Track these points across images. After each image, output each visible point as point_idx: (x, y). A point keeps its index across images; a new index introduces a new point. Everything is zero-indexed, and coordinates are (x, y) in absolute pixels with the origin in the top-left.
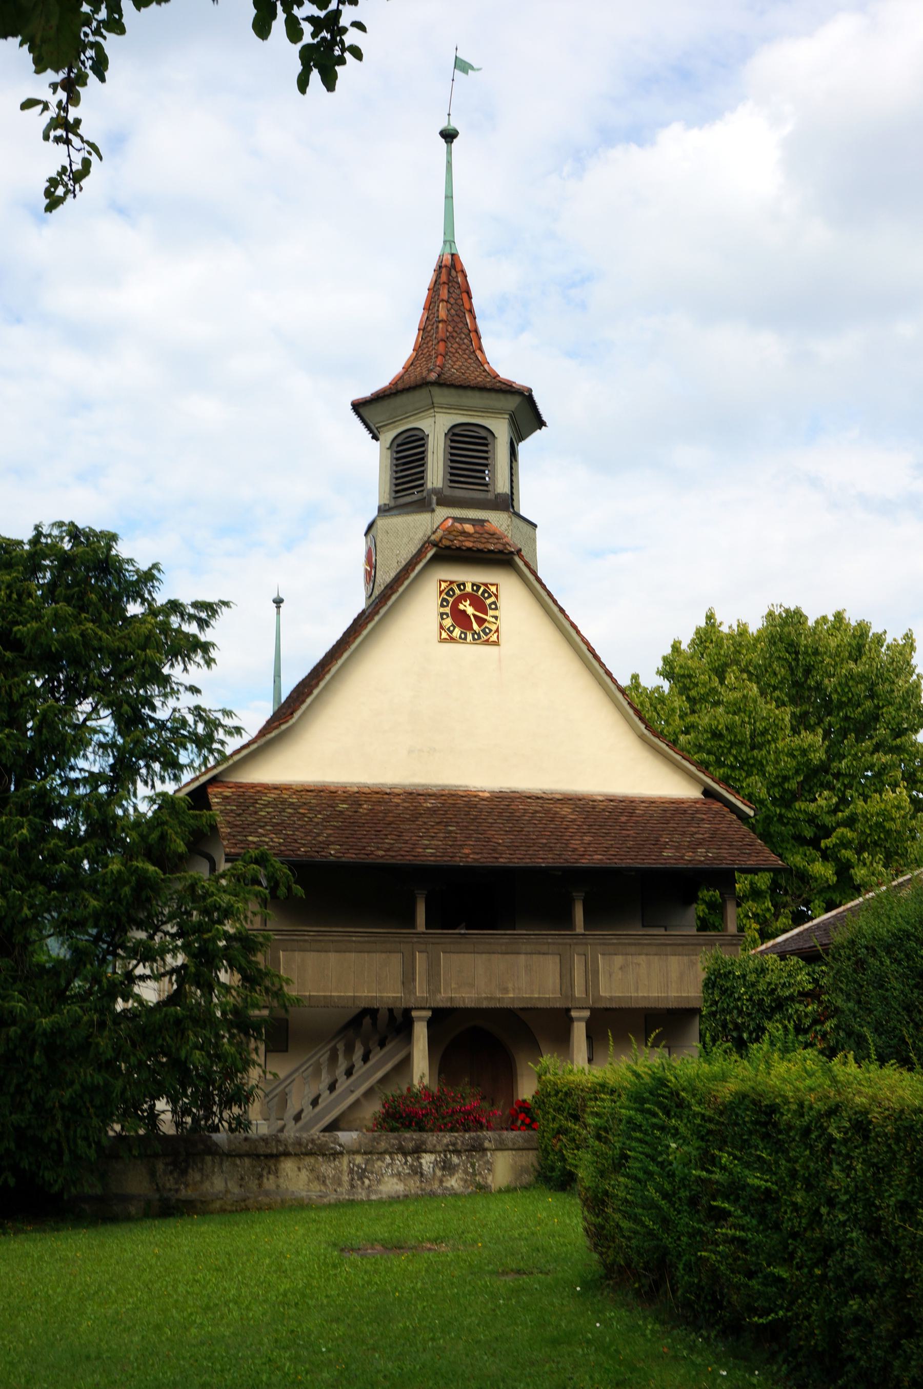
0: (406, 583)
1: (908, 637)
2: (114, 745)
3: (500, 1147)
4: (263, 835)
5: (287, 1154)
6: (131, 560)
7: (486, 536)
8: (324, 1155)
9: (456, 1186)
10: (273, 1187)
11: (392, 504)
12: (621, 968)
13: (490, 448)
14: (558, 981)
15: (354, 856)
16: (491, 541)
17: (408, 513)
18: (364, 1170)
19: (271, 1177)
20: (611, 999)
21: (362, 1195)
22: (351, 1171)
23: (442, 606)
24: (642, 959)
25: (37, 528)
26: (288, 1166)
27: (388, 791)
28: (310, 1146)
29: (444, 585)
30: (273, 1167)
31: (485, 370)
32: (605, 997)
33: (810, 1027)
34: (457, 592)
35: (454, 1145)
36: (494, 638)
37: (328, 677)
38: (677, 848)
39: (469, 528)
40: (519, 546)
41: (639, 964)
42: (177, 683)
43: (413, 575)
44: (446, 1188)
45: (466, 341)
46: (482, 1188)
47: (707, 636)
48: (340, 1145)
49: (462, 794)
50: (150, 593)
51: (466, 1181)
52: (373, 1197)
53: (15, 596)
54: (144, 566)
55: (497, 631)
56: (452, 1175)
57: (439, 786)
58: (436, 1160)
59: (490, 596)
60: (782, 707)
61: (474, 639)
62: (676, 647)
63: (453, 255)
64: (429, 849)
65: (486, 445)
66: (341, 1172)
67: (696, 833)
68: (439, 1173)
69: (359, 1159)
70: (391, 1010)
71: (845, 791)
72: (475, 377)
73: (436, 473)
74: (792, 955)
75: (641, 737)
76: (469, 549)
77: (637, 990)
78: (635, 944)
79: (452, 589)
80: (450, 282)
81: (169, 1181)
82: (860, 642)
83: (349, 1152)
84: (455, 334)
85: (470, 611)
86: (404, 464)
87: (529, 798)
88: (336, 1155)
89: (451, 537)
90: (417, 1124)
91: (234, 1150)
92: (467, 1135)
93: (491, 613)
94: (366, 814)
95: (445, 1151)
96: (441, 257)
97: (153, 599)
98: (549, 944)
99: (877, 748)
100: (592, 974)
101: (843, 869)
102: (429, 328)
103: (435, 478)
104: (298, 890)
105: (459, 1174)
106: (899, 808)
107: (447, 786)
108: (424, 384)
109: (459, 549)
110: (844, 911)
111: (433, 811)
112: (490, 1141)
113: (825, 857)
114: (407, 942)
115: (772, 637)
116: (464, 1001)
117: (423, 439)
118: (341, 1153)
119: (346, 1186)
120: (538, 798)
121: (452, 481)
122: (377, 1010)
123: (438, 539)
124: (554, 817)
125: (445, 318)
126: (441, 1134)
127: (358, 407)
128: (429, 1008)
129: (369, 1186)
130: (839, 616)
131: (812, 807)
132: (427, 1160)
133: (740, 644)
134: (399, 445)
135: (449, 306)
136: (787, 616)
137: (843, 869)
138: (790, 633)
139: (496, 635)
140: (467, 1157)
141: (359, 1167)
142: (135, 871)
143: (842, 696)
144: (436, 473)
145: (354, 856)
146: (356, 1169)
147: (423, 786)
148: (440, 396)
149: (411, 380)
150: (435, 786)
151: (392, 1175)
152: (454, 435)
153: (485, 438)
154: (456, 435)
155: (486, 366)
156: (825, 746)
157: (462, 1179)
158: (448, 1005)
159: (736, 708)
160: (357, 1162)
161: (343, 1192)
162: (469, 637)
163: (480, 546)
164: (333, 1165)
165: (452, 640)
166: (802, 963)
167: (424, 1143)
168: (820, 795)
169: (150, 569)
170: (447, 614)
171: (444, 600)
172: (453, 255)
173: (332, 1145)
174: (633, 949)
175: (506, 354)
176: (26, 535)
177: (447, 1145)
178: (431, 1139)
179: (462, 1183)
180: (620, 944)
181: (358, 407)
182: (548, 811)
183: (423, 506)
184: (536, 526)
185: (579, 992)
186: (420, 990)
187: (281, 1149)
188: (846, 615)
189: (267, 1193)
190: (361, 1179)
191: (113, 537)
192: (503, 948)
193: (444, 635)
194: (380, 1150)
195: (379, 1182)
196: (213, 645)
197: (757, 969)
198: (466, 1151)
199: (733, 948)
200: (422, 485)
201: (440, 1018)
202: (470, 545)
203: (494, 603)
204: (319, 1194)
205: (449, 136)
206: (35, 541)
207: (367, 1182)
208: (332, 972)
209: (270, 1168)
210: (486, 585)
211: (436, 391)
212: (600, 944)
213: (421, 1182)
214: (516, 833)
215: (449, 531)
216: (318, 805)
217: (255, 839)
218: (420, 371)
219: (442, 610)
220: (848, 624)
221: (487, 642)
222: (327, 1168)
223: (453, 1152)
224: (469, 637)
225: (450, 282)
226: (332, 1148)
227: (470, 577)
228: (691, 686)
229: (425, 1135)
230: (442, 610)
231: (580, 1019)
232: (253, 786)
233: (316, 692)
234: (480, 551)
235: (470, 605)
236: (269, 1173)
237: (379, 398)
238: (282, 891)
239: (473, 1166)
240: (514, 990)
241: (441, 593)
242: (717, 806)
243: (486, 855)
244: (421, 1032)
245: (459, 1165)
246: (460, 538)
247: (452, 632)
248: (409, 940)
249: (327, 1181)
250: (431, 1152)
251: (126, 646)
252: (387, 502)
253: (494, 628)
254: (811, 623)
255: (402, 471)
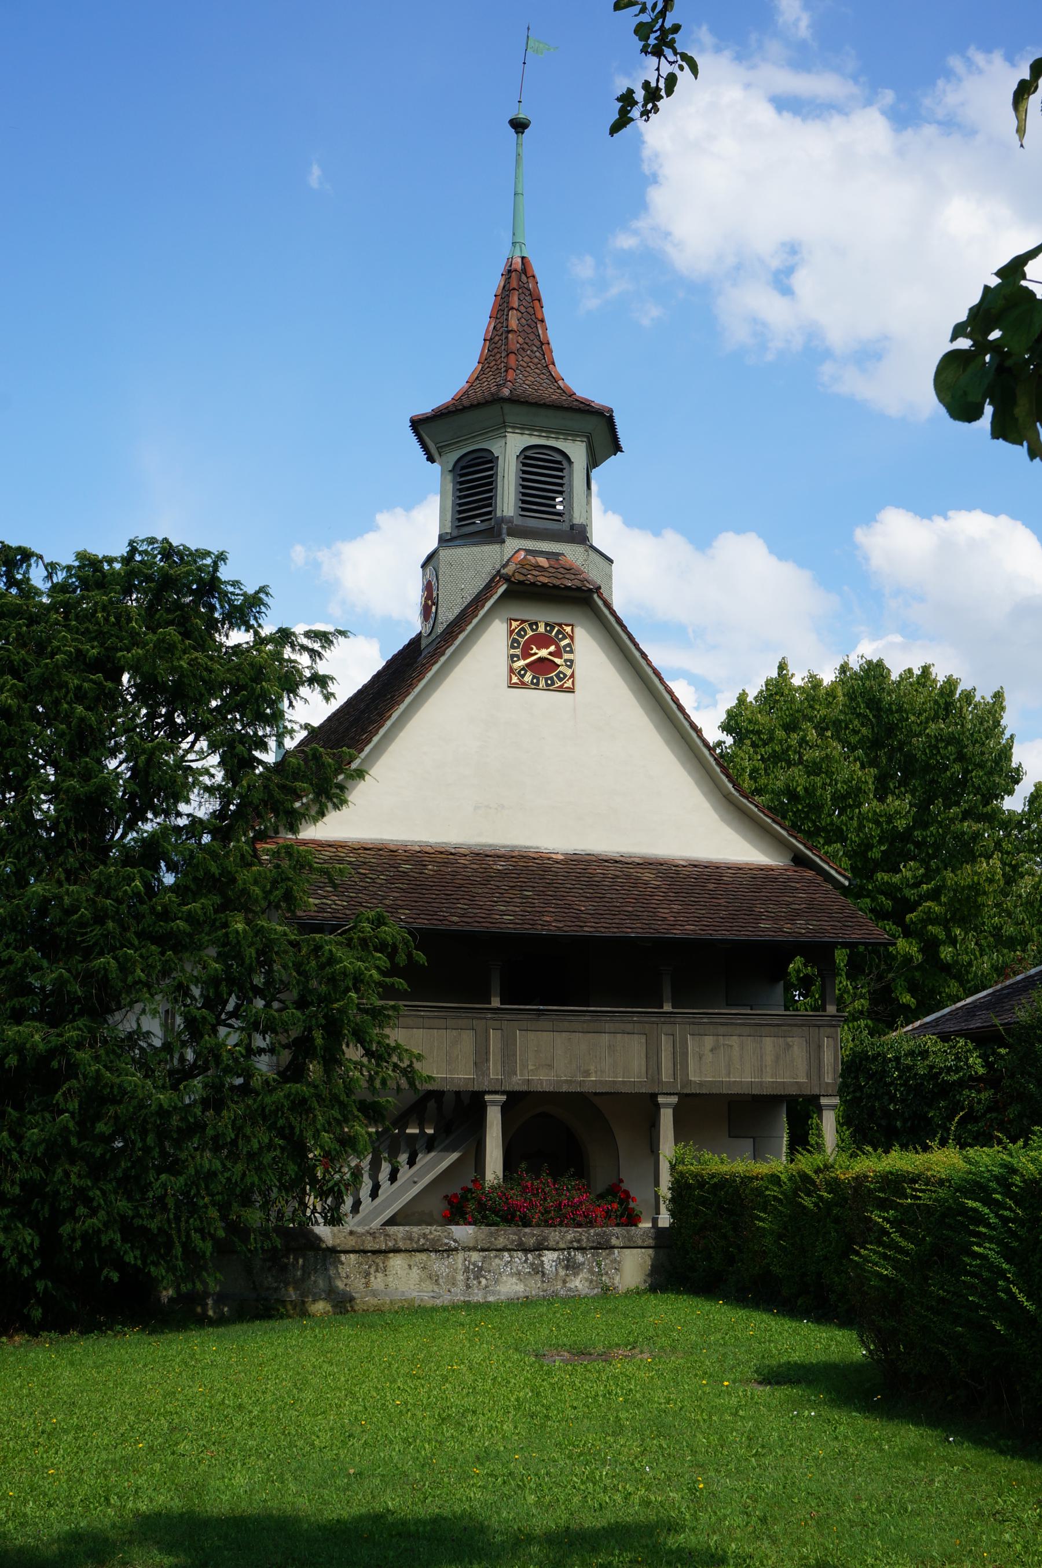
0: (475, 621)
1: (998, 696)
2: (219, 787)
3: (628, 1244)
4: (325, 897)
5: (396, 1251)
6: (238, 582)
7: (562, 570)
8: (437, 1251)
9: (580, 1287)
10: (382, 1286)
11: (455, 533)
12: (712, 1050)
13: (565, 473)
14: (644, 1062)
15: (426, 922)
16: (567, 576)
17: (474, 544)
18: (481, 1269)
19: (379, 1275)
20: (701, 1084)
21: (478, 1297)
22: (467, 1270)
23: (513, 647)
24: (734, 1041)
25: (131, 543)
26: (397, 1262)
27: (453, 851)
28: (422, 1241)
29: (514, 624)
30: (381, 1265)
31: (559, 388)
32: (695, 1082)
33: (984, 1115)
34: (542, 629)
35: (579, 1241)
36: (569, 684)
37: (389, 723)
38: (775, 919)
39: (543, 561)
40: (599, 582)
41: (731, 1046)
42: (290, 721)
43: (482, 613)
44: (570, 1290)
45: (537, 354)
46: (606, 1290)
47: (777, 690)
48: (455, 1241)
49: (533, 855)
50: (256, 619)
51: (591, 1282)
52: (491, 1299)
53: (112, 619)
54: (251, 590)
55: (572, 676)
56: (575, 1274)
57: (508, 846)
58: (558, 1258)
59: (564, 638)
60: (864, 766)
61: (547, 685)
62: (742, 699)
63: (523, 258)
64: (507, 916)
65: (561, 470)
66: (455, 1270)
67: (792, 903)
68: (562, 1272)
69: (475, 1256)
70: (458, 1093)
71: (929, 862)
72: (550, 394)
73: (507, 500)
74: (957, 1036)
75: (727, 797)
76: (544, 585)
77: (729, 1075)
78: (726, 1024)
79: (523, 629)
80: (519, 291)
81: (267, 1276)
82: (947, 700)
83: (464, 1249)
84: (525, 346)
85: (543, 653)
86: (468, 489)
87: (606, 861)
88: (450, 1251)
89: (524, 571)
90: (522, 1219)
91: (339, 1245)
92: (592, 1231)
93: (566, 656)
94: (432, 876)
95: (569, 1248)
96: (510, 261)
97: (260, 626)
98: (634, 1022)
99: (966, 815)
100: (680, 1058)
101: (930, 947)
102: (497, 338)
103: (505, 505)
104: (421, 957)
105: (584, 1274)
106: (991, 881)
107: (516, 847)
108: (495, 400)
109: (533, 584)
110: (1002, 989)
111: (503, 874)
112: (617, 1238)
113: (907, 934)
114: (481, 1018)
115: (854, 692)
116: (542, 1084)
117: (491, 461)
118: (456, 1249)
119: (461, 1286)
120: (616, 862)
121: (523, 509)
122: (443, 1092)
123: (510, 573)
124: (637, 883)
125: (515, 328)
126: (564, 1229)
127: (417, 425)
128: (503, 1093)
129: (487, 1287)
130: (926, 670)
131: (896, 879)
132: (549, 1258)
133: (813, 700)
134: (463, 468)
135: (520, 314)
136: (869, 668)
137: (930, 947)
138: (872, 687)
139: (571, 681)
140: (593, 1255)
141: (474, 1264)
142: (259, 931)
143: (930, 758)
144: (507, 500)
145: (426, 922)
146: (471, 1267)
147: (490, 846)
148: (512, 414)
149: (478, 396)
150: (504, 847)
151: (512, 1275)
152: (526, 457)
153: (560, 463)
154: (528, 457)
155: (560, 382)
156: (912, 813)
157: (587, 1280)
158: (524, 1088)
159: (814, 769)
160: (473, 1260)
161: (458, 1295)
162: (542, 683)
163: (557, 582)
164: (446, 1263)
165: (523, 685)
166: (970, 1046)
167: (546, 1239)
168: (904, 866)
169: (257, 593)
170: (517, 656)
171: (515, 640)
172: (523, 258)
173: (446, 1241)
174: (722, 1030)
175: (581, 370)
176: (121, 550)
177: (572, 1242)
178: (554, 1235)
179: (587, 1284)
180: (711, 1023)
181: (417, 425)
182: (628, 876)
183: (493, 535)
184: (611, 561)
185: (666, 1076)
186: (494, 1071)
187: (390, 1244)
188: (933, 670)
189: (374, 1294)
190: (477, 1278)
191: (221, 557)
192: (585, 1025)
193: (515, 680)
194: (499, 1247)
195: (497, 1282)
196: (332, 679)
197: (914, 1052)
198: (592, 1248)
199: (833, 1029)
200: (490, 513)
201: (516, 1103)
202: (546, 580)
203: (569, 645)
204: (432, 1294)
205: (519, 126)
206: (127, 560)
207: (484, 1281)
208: (441, 1051)
209: (377, 1265)
210: (560, 625)
211: (507, 408)
212: (690, 1024)
213: (543, 1282)
214: (598, 900)
215: (522, 564)
216: (378, 865)
217: (317, 901)
218: (489, 386)
219: (512, 651)
220: (935, 681)
221: (561, 689)
222: (439, 1265)
223: (577, 1249)
224: (542, 683)
225: (519, 291)
226: (446, 1244)
227: (543, 616)
228: (760, 743)
229: (547, 1231)
230: (512, 651)
231: (667, 1105)
232: (314, 842)
233: (376, 739)
234: (555, 587)
235: (538, 649)
236: (377, 1271)
237: (441, 415)
238: (402, 959)
239: (599, 1265)
240: (596, 1072)
241: (512, 632)
242: (809, 874)
243: (570, 924)
244: (494, 1118)
245: (584, 1264)
246: (534, 573)
247: (523, 676)
248: (482, 1016)
249: (441, 1281)
250: (555, 1250)
251: (238, 678)
252: (449, 531)
253: (569, 672)
254: (894, 676)
255: (466, 496)
